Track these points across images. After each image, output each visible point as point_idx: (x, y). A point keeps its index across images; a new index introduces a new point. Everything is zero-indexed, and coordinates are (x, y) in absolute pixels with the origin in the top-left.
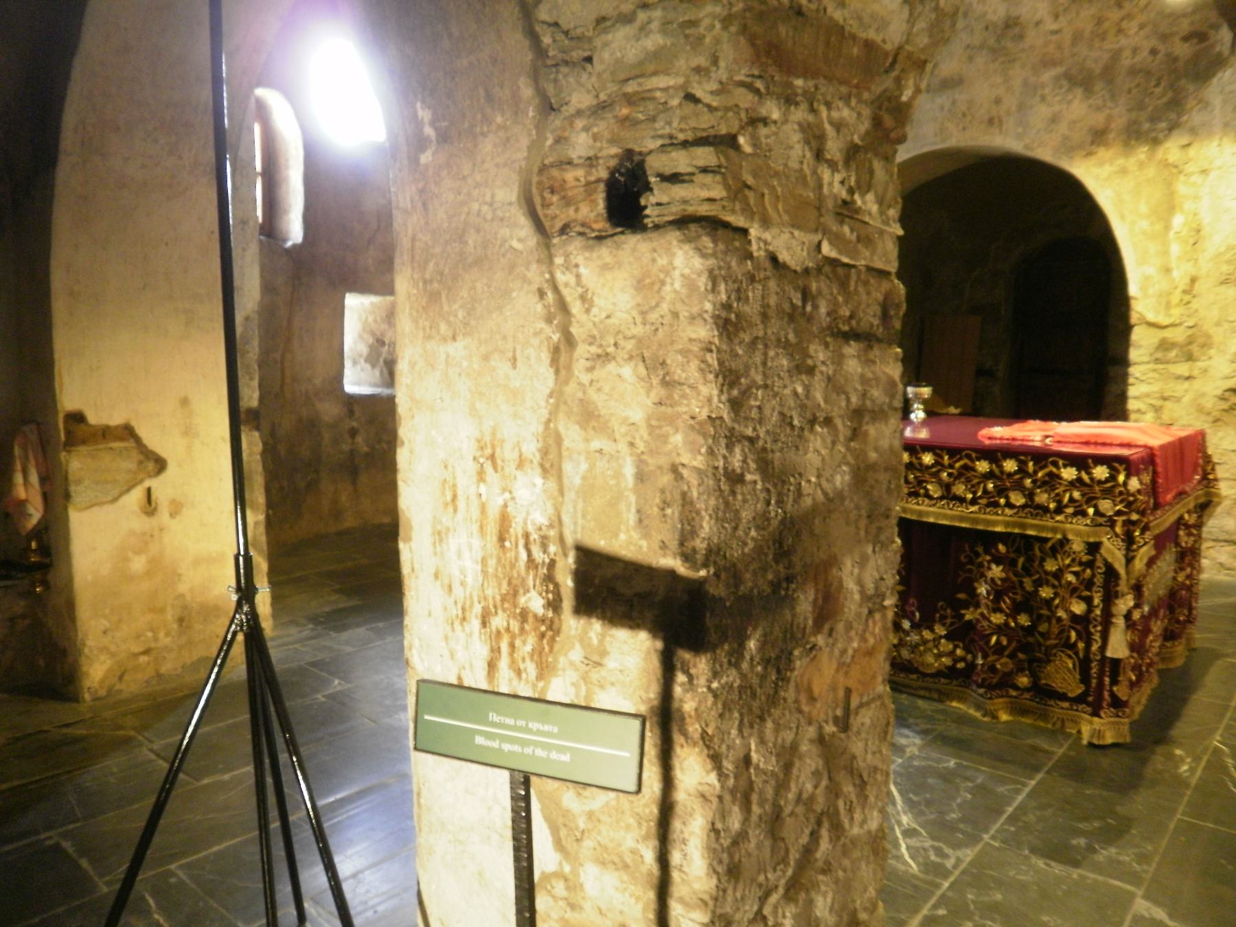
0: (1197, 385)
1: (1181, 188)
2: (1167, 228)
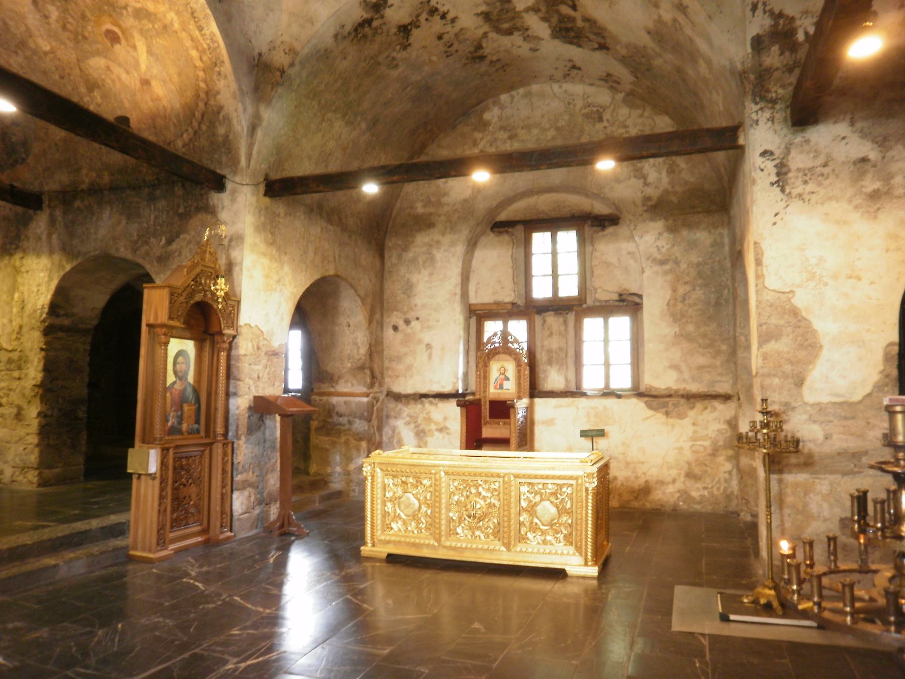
0: (22, 382)
1: (20, 280)
2: (12, 299)
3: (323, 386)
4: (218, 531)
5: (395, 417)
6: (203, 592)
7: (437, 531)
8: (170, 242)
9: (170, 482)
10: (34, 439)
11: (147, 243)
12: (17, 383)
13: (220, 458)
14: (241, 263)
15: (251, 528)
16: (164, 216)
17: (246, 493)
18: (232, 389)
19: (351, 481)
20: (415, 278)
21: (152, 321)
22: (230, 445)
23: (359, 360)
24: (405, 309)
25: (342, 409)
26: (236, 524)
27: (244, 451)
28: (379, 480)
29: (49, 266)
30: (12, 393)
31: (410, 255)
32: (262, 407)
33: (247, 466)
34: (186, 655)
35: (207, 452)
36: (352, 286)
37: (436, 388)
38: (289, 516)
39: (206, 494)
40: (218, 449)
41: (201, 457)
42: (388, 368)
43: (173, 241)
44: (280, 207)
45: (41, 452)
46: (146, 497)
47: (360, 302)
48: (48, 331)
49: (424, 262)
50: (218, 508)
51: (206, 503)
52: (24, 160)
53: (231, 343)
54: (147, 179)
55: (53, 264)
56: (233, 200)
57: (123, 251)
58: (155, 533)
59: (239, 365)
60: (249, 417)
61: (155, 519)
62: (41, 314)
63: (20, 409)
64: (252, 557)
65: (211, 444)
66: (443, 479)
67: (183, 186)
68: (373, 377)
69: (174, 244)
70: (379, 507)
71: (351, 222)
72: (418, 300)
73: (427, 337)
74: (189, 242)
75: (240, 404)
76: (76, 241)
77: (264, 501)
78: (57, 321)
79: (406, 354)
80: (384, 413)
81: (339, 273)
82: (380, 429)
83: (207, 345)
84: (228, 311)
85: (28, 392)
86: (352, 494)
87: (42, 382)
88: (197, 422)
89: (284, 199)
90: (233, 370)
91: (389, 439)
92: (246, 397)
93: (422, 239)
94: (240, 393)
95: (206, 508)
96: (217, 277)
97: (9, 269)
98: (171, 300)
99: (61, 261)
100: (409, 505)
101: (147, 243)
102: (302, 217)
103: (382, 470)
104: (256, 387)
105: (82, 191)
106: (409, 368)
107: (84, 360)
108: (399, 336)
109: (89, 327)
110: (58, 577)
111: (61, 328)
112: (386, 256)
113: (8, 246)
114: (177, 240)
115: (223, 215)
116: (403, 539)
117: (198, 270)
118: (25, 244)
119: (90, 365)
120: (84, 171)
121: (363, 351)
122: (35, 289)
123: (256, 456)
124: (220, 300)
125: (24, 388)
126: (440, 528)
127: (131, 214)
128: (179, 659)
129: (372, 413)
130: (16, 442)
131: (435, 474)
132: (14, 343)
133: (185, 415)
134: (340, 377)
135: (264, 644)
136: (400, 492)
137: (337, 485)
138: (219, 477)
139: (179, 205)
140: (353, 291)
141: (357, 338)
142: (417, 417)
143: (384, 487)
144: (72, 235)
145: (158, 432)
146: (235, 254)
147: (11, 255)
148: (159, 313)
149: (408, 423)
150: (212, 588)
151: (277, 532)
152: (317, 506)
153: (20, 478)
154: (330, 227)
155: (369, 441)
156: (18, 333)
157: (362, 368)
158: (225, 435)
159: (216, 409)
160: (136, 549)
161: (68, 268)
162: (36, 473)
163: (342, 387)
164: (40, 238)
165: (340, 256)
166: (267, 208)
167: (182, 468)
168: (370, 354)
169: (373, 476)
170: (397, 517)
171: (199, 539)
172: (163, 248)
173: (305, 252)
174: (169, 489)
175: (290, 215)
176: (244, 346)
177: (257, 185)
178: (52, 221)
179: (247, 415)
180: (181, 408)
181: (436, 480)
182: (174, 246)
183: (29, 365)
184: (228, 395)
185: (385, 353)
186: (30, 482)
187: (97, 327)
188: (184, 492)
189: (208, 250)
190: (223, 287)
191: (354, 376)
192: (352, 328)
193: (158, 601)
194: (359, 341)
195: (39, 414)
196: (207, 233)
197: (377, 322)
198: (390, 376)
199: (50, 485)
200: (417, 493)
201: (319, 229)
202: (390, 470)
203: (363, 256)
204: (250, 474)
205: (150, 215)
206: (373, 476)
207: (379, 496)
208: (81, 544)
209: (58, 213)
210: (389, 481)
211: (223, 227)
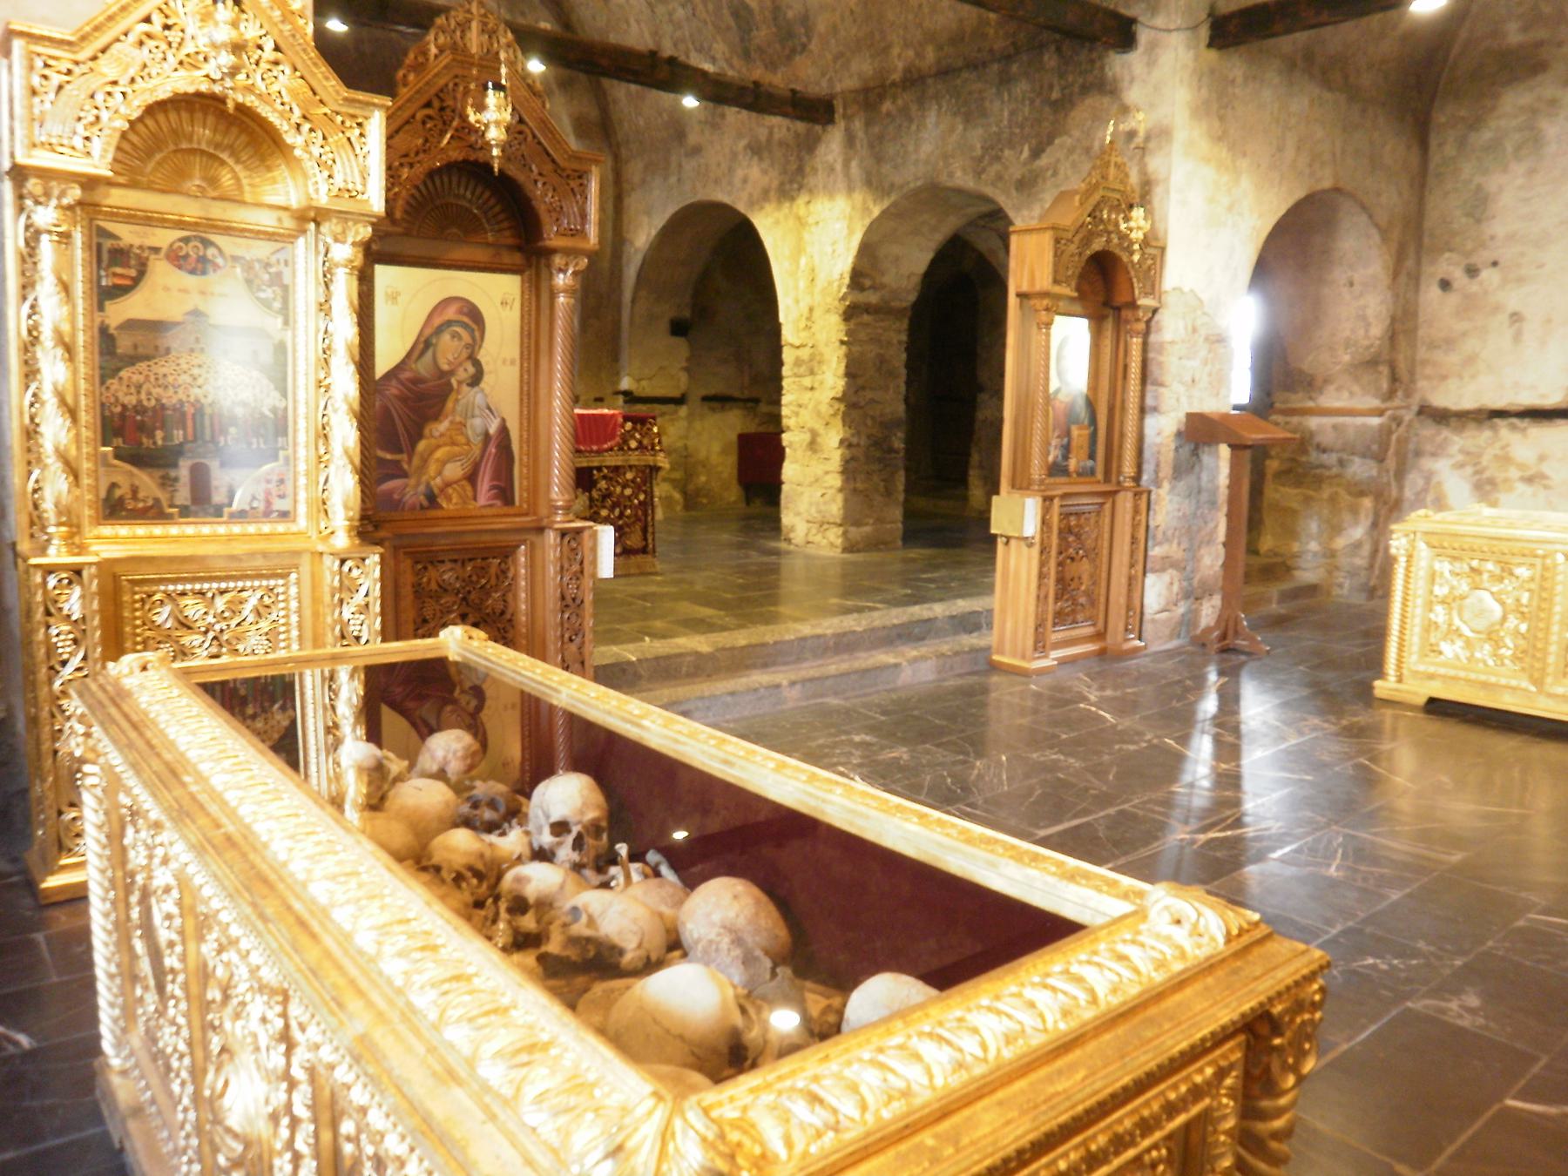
0: (816, 394)
1: (806, 236)
2: (798, 267)
3: (1293, 397)
4: (1120, 638)
5: (1434, 455)
6: (1114, 726)
7: (1537, 665)
8: (1036, 153)
9: (1054, 553)
10: (836, 481)
11: (998, 158)
12: (809, 394)
13: (1128, 517)
14: (1167, 179)
15: (1171, 637)
16: (1027, 110)
17: (1166, 577)
18: (1149, 401)
19: (1337, 568)
20: (1493, 182)
21: (1025, 288)
22: (1144, 497)
23: (1368, 347)
24: (1469, 246)
25: (1327, 438)
26: (1147, 627)
27: (1168, 506)
28: (1423, 563)
29: (848, 210)
30: (802, 411)
31: (1487, 135)
32: (1200, 432)
33: (1170, 533)
34: (1111, 811)
35: (1108, 506)
36: (1364, 207)
37: (1527, 399)
38: (1237, 621)
39: (1104, 575)
40: (1125, 502)
41: (1098, 513)
42: (1425, 363)
43: (1043, 151)
44: (1236, 65)
45: (846, 500)
46: (1018, 572)
47: (1377, 237)
48: (850, 313)
49: (1518, 148)
50: (1123, 601)
51: (1103, 591)
52: (804, 47)
53: (1148, 322)
54: (996, 47)
55: (853, 208)
56: (1151, 63)
57: (962, 178)
58: (1032, 630)
59: (1161, 359)
60: (1177, 449)
61: (1032, 608)
62: (840, 287)
63: (814, 435)
64: (1180, 682)
65: (1115, 492)
66: (1561, 568)
67: (1058, 50)
68: (1394, 378)
69: (1044, 156)
70: (1418, 611)
71: (1366, 80)
72: (1498, 228)
73: (1513, 299)
74: (1071, 151)
75: (1162, 429)
76: (886, 168)
77: (1194, 594)
78: (862, 298)
79: (1464, 334)
80: (1411, 446)
81: (1341, 185)
82: (1400, 474)
83: (1109, 326)
84: (1145, 267)
85: (825, 409)
86: (1336, 591)
87: (845, 393)
88: (1092, 456)
89: (1242, 48)
90: (1153, 368)
91: (1417, 494)
92: (1173, 415)
93: (1514, 100)
94: (1164, 407)
95: (1102, 599)
96: (1131, 207)
97: (791, 222)
98: (1056, 250)
99: (865, 202)
100: (1481, 612)
101: (998, 158)
102: (1276, 80)
103: (1431, 546)
104: (1190, 397)
105: (894, 84)
106: (1470, 360)
107: (899, 359)
108: (1453, 299)
109: (904, 304)
110: (900, 683)
111: (867, 309)
112: (1433, 142)
113: (787, 187)
114: (1048, 150)
115: (1133, 95)
116: (1462, 674)
117: (1097, 197)
118: (811, 181)
119: (907, 366)
120: (896, 51)
121: (1377, 330)
122: (829, 250)
123: (1184, 515)
124: (1136, 247)
125: (819, 403)
126: (1543, 660)
127: (971, 113)
128: (1102, 814)
129: (1388, 445)
130: (811, 485)
131: (1544, 557)
132: (804, 334)
133: (1074, 444)
134: (1327, 381)
135: (1228, 813)
136: (1464, 587)
137: (1308, 574)
138: (1127, 548)
139: (1051, 87)
140: (1364, 219)
141: (1365, 307)
142: (1480, 455)
143: (1433, 577)
144: (879, 159)
145: (1037, 470)
146: (1155, 164)
147: (793, 199)
148: (1037, 274)
149: (1461, 466)
150: (1126, 723)
151: (1216, 646)
152: (1275, 608)
153: (818, 538)
154: (1327, 95)
155: (1379, 495)
156: (808, 319)
157: (1372, 363)
158: (1137, 478)
159: (1122, 435)
160: (1001, 652)
161: (876, 211)
162: (841, 530)
163: (1331, 399)
164: (832, 169)
165: (1343, 152)
166: (1212, 71)
167: (1070, 531)
168: (1392, 337)
169: (1410, 557)
170: (1453, 633)
171: (1090, 647)
172: (1025, 164)
173: (1280, 149)
174: (1053, 564)
175: (1254, 78)
176: (1171, 327)
177: (1194, 28)
178: (850, 140)
179: (1173, 446)
180: (1068, 433)
181: (1545, 568)
182: (1044, 161)
183: (824, 368)
184: (1142, 411)
185: (1421, 333)
186: (832, 545)
187: (915, 305)
188: (1072, 569)
189: (1113, 159)
190: (1142, 223)
191: (1357, 379)
192: (1357, 288)
193: (1050, 730)
194: (1370, 312)
195: (842, 442)
196: (1111, 129)
197: (1409, 274)
198: (1428, 378)
199: (859, 551)
200: (1501, 592)
201: (1306, 102)
202: (1442, 545)
203: (1388, 148)
204: (1175, 545)
205: (1002, 110)
206: (1410, 557)
207: (1420, 592)
208: (923, 639)
209: (858, 125)
210: (1444, 567)
211: (1141, 116)
